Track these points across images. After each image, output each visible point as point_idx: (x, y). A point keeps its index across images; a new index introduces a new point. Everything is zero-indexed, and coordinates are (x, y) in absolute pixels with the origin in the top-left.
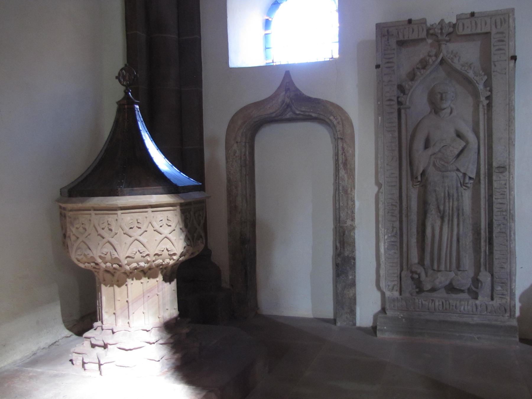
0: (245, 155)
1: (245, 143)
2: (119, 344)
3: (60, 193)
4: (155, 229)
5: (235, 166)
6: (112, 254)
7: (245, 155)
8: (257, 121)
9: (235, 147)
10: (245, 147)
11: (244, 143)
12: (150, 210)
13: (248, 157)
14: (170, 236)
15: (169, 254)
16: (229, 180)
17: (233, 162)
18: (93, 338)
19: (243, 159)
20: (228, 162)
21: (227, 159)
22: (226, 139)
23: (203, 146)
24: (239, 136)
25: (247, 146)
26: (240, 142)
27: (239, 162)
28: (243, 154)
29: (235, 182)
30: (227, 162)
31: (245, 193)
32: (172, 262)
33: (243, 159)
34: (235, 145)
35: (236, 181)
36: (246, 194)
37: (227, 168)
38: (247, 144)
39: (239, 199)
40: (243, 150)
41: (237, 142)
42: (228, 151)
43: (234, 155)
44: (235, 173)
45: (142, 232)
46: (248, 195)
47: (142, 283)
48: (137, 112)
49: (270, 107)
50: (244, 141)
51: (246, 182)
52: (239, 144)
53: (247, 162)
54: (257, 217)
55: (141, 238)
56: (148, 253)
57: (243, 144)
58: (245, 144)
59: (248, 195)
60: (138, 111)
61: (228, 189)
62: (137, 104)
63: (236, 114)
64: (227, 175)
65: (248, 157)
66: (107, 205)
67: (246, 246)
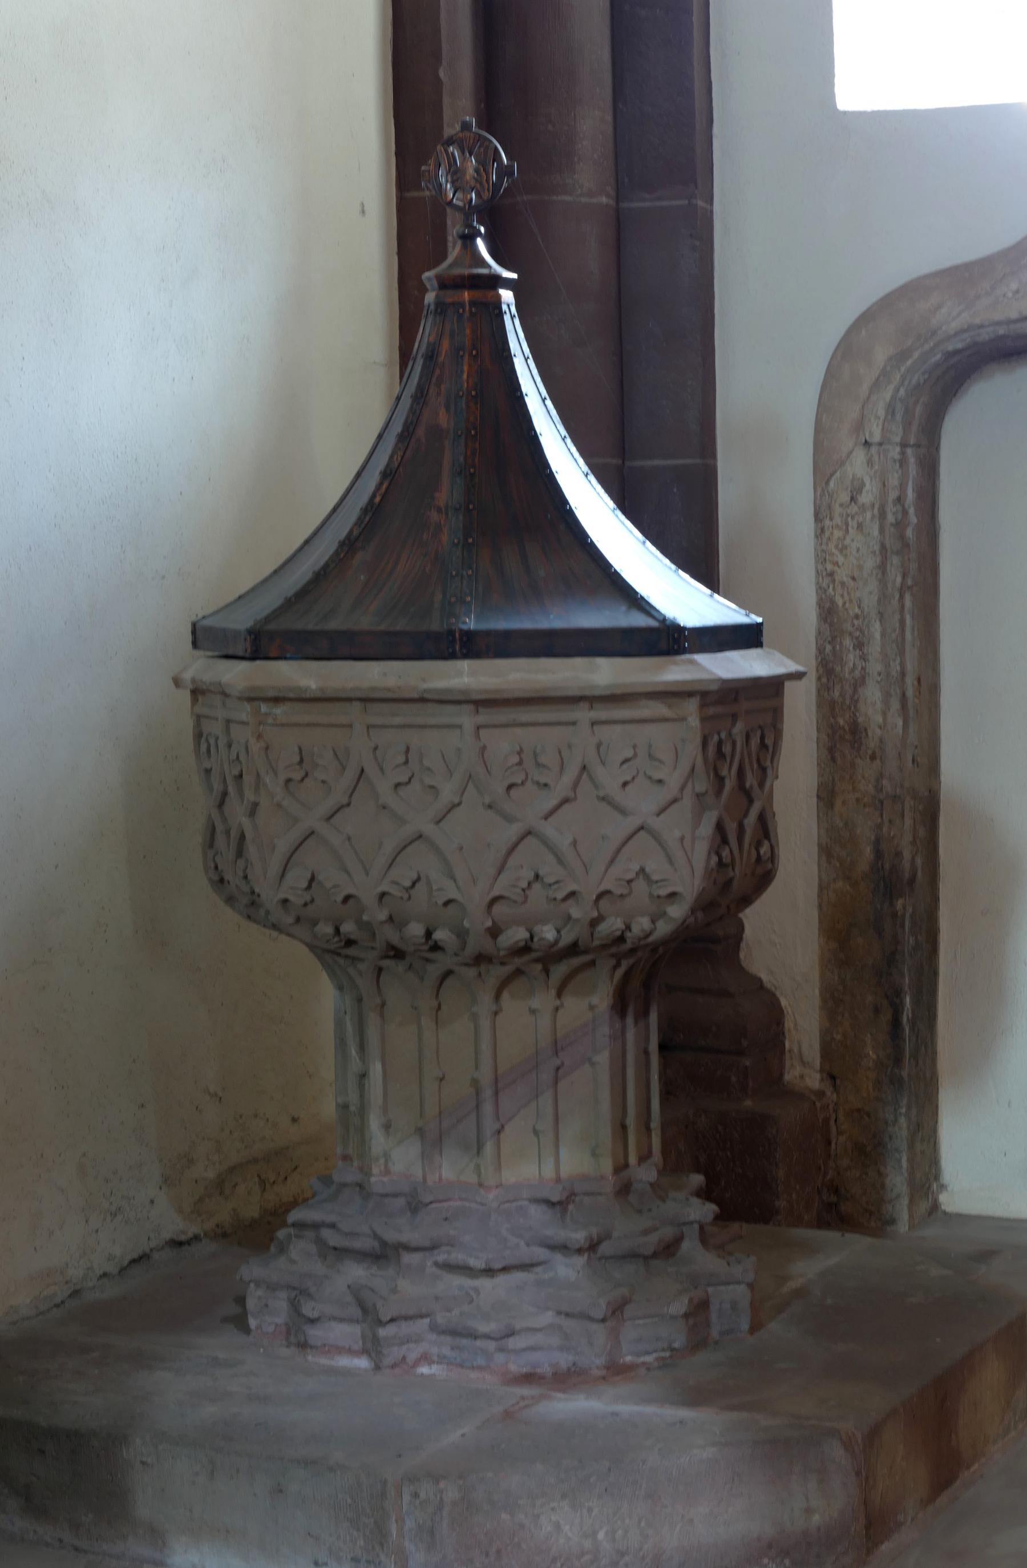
0: (899, 500)
1: (904, 445)
2: (444, 1248)
3: (190, 638)
4: (601, 794)
5: (858, 550)
6: (435, 887)
7: (899, 500)
8: (956, 352)
9: (857, 465)
10: (903, 462)
11: (898, 449)
12: (583, 714)
13: (911, 511)
14: (655, 823)
15: (651, 895)
16: (827, 612)
17: (847, 531)
18: (333, 1226)
19: (890, 518)
20: (823, 530)
21: (818, 517)
22: (819, 429)
23: (714, 456)
24: (877, 418)
25: (912, 460)
26: (880, 444)
27: (876, 532)
28: (893, 495)
29: (856, 622)
30: (820, 533)
31: (898, 668)
32: (663, 929)
33: (890, 518)
34: (860, 456)
35: (857, 617)
36: (903, 674)
37: (821, 558)
38: (909, 451)
39: (872, 694)
40: (894, 480)
41: (866, 443)
42: (827, 482)
43: (853, 499)
44: (853, 579)
45: (554, 802)
46: (910, 681)
47: (533, 1012)
48: (507, 318)
49: (1017, 292)
50: (898, 439)
51: (902, 622)
52: (874, 450)
53: (909, 533)
54: (942, 778)
55: (548, 829)
56: (573, 887)
57: (895, 452)
58: (903, 453)
59: (910, 681)
60: (512, 317)
61: (820, 650)
62: (507, 284)
63: (866, 318)
64: (820, 589)
65: (911, 511)
66: (425, 691)
67: (899, 903)
